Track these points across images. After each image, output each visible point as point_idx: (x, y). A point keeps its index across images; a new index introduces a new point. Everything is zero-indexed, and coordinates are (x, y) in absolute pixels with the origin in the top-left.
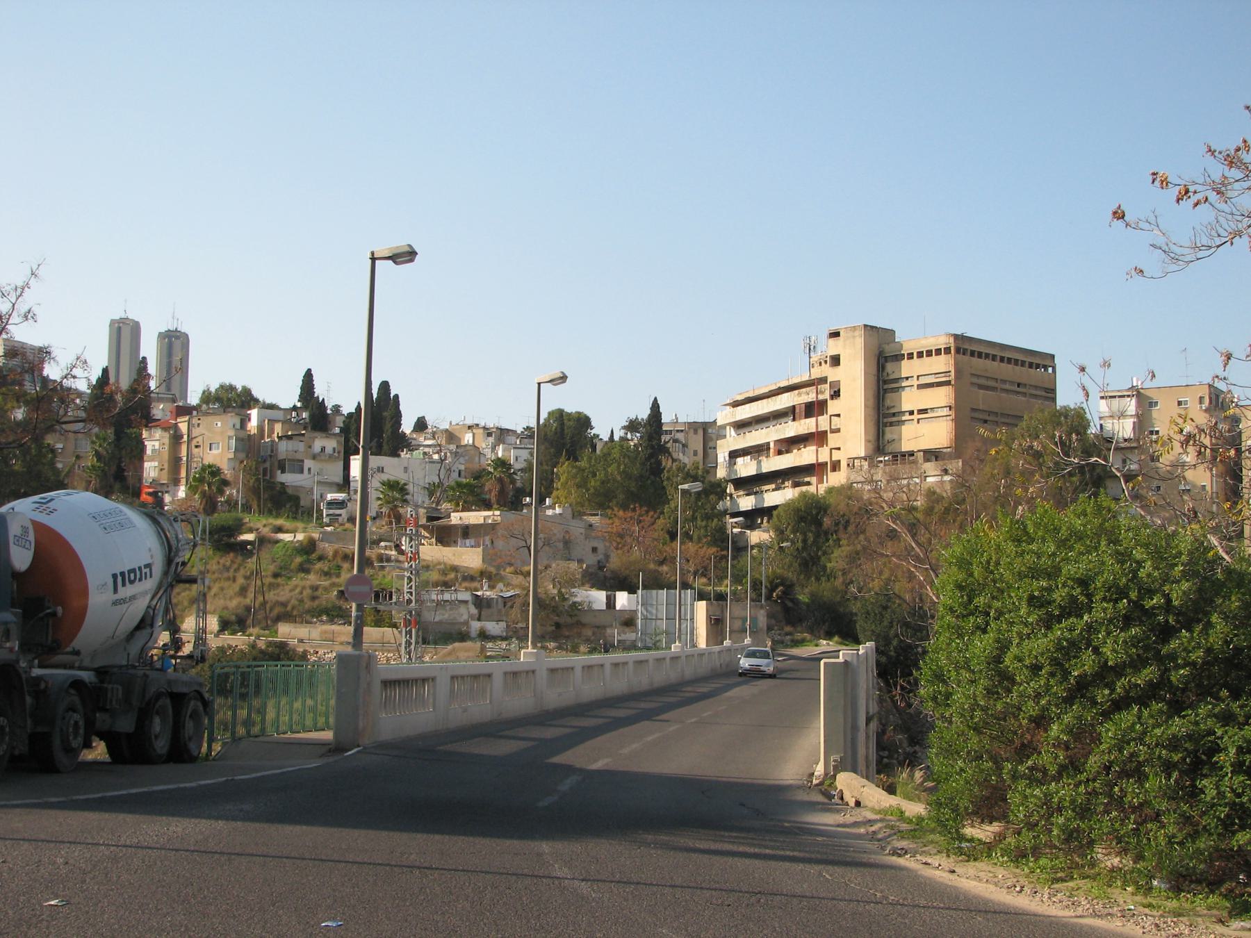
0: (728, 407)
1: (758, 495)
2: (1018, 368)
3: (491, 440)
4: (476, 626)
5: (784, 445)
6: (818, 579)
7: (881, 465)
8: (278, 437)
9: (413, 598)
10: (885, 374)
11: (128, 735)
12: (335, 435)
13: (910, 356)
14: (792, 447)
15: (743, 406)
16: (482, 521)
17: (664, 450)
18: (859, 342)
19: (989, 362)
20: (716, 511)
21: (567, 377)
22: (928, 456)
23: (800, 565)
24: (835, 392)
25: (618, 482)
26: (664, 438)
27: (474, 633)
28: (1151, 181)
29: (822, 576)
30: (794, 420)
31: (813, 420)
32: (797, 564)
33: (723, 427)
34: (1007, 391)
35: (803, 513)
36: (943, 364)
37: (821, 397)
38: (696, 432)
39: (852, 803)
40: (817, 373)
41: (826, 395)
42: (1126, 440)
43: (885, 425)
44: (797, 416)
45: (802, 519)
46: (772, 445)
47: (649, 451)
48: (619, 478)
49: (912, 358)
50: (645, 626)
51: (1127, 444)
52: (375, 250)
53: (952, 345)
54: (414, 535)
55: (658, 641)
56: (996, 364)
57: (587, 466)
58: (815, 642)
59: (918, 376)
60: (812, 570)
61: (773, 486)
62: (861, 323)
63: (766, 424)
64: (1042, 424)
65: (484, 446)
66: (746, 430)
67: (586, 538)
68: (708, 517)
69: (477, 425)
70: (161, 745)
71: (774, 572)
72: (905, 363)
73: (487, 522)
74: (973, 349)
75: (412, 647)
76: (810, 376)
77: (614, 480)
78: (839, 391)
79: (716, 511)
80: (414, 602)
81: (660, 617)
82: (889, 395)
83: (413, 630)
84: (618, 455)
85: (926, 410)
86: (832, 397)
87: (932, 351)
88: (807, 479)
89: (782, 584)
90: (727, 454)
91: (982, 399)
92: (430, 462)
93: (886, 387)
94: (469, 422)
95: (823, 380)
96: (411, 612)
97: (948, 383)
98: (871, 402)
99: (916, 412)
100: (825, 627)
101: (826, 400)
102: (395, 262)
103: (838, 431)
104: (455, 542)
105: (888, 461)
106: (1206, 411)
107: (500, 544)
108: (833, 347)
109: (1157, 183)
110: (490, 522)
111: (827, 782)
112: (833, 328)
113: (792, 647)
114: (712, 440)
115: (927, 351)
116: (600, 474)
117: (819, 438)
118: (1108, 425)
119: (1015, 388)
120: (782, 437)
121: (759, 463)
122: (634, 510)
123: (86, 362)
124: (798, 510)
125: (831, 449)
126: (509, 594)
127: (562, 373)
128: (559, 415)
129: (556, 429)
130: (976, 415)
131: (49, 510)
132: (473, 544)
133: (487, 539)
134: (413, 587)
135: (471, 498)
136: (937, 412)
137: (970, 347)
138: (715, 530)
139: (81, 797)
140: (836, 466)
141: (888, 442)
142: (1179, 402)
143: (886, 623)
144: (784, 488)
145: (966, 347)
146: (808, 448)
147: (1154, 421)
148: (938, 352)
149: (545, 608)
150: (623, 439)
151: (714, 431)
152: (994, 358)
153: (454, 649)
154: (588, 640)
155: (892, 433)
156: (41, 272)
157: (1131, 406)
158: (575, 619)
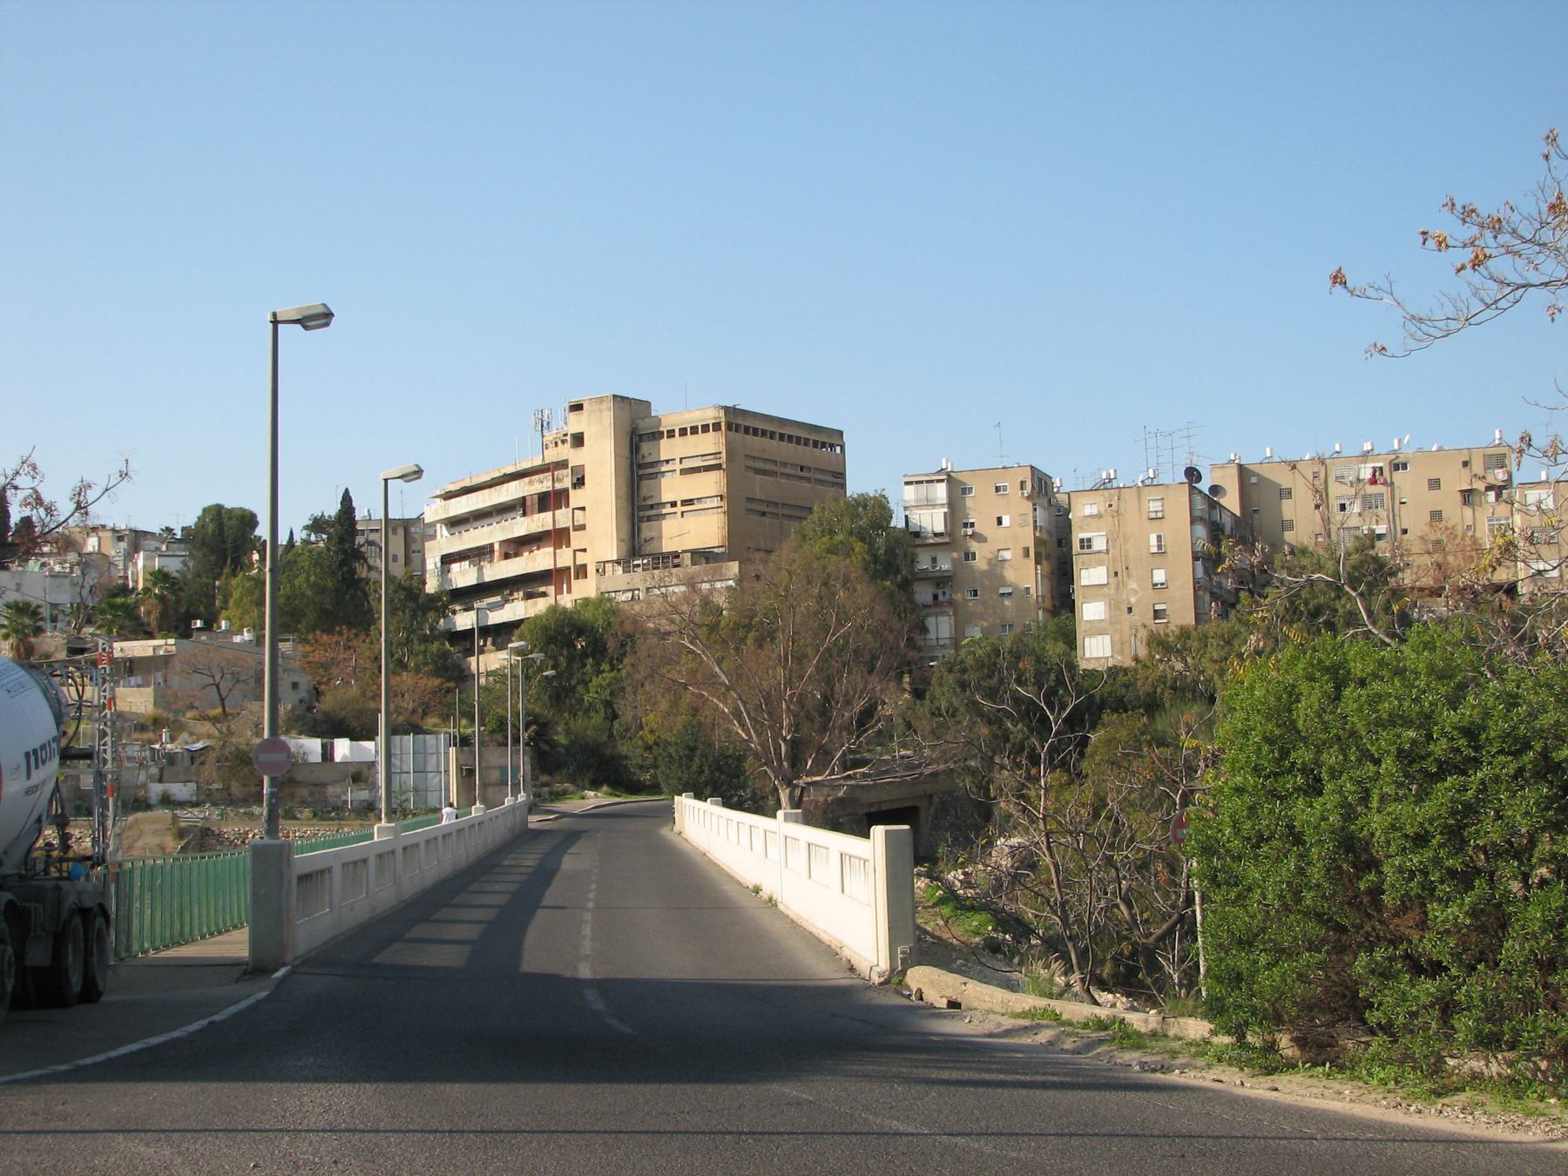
0: (438, 500)
2: (801, 448)
3: (123, 545)
4: (156, 789)
5: (512, 546)
7: (640, 569)
10: (640, 456)
13: (671, 434)
14: (523, 548)
15: (458, 499)
16: (150, 653)
17: (358, 555)
18: (608, 417)
19: (766, 441)
23: (550, 697)
24: (578, 479)
25: (308, 598)
26: (360, 540)
27: (154, 799)
28: (1421, 242)
29: (579, 710)
30: (524, 514)
31: (550, 514)
32: (546, 697)
33: (433, 524)
34: (789, 476)
36: (711, 443)
37: (558, 486)
38: (395, 531)
39: (943, 1003)
40: (552, 455)
41: (567, 483)
42: (936, 535)
43: (641, 520)
44: (528, 510)
45: (551, 640)
46: (497, 547)
47: (341, 557)
49: (674, 436)
51: (939, 540)
52: (278, 311)
53: (723, 420)
54: (108, 675)
56: (774, 443)
59: (681, 459)
62: (609, 394)
63: (489, 521)
64: (837, 516)
65: (113, 553)
69: (104, 527)
70: (76, 982)
72: (664, 443)
73: (157, 654)
76: (543, 459)
77: (303, 595)
78: (583, 477)
80: (110, 762)
82: (645, 483)
83: (111, 799)
85: (692, 500)
86: (575, 486)
87: (697, 427)
88: (542, 589)
89: (535, 722)
90: (438, 560)
91: (760, 486)
92: (51, 576)
93: (641, 472)
95: (563, 464)
97: (717, 467)
98: (624, 489)
99: (679, 503)
100: (590, 775)
101: (566, 490)
102: (306, 328)
103: (582, 527)
105: (648, 564)
106: (1028, 498)
107: (176, 681)
108: (575, 424)
109: (1431, 243)
110: (162, 653)
111: (895, 980)
112: (575, 400)
113: (552, 801)
117: (558, 537)
120: (510, 536)
121: (480, 569)
122: (340, 633)
123: (34, 468)
124: (546, 628)
125: (575, 551)
126: (199, 745)
127: (417, 466)
129: (213, 531)
132: (140, 682)
134: (109, 744)
136: (705, 502)
137: (744, 423)
139: (89, 1061)
140: (582, 571)
141: (646, 541)
142: (997, 488)
143: (694, 768)
145: (739, 422)
146: (542, 550)
147: (968, 511)
148: (705, 428)
150: (306, 542)
151: (418, 530)
153: (136, 820)
154: (304, 803)
157: (941, 491)
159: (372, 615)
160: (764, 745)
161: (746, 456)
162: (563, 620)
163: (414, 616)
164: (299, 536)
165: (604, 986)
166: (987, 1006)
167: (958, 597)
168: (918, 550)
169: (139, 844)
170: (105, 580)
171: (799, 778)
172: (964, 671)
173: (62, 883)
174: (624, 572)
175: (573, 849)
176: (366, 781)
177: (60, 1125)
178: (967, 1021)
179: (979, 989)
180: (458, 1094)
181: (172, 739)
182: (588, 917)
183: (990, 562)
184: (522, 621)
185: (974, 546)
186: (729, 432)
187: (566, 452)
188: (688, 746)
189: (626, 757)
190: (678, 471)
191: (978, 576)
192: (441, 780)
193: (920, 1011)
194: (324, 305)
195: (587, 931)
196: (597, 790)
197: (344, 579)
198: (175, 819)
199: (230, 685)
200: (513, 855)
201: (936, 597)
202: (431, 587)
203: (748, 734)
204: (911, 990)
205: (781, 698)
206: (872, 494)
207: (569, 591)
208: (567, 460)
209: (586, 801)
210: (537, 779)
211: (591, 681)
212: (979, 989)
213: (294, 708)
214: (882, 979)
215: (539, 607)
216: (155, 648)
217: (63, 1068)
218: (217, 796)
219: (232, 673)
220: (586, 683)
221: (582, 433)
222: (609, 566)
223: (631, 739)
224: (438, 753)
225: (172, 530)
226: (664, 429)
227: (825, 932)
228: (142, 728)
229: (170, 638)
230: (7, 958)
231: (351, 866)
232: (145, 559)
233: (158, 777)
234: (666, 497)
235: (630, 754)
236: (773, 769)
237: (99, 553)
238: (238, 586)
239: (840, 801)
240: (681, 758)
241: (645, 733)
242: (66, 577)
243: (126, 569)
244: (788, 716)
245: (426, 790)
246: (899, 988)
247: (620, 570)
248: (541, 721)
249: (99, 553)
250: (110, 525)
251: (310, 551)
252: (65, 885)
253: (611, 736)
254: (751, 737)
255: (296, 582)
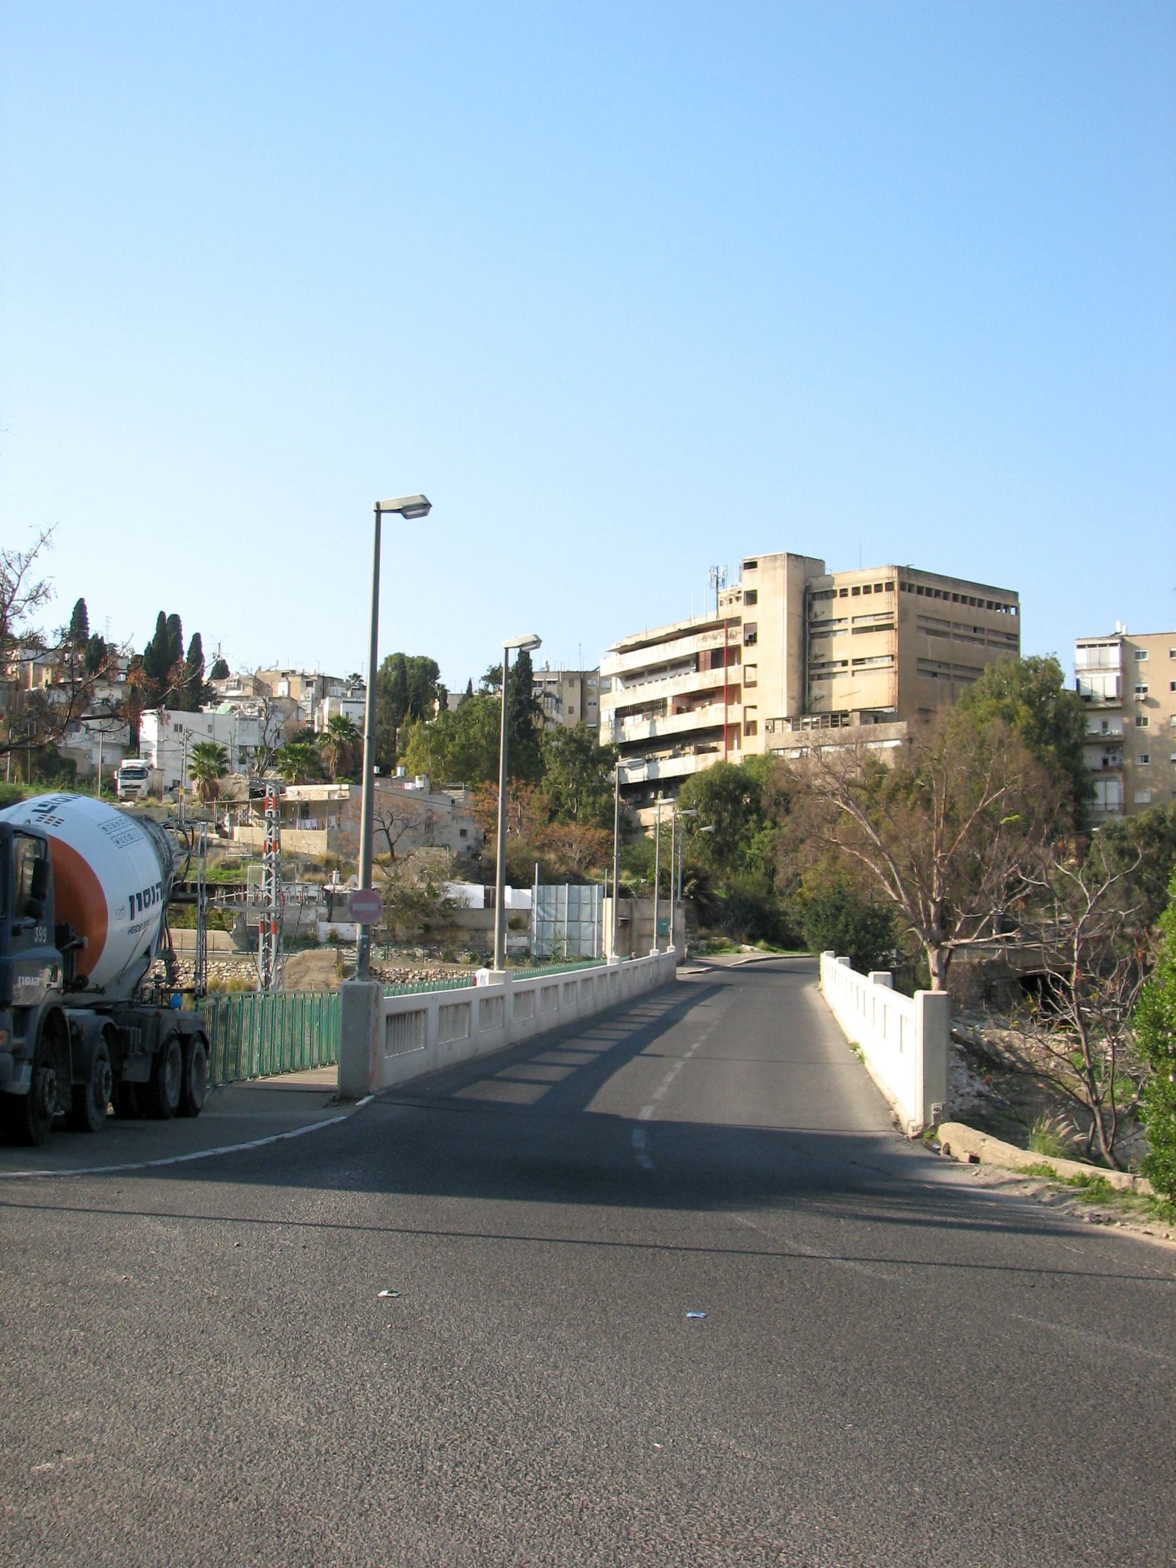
0: (614, 654)
1: (652, 764)
2: (974, 609)
3: (311, 690)
4: (325, 928)
5: (685, 701)
6: (735, 869)
7: (808, 728)
8: (47, 685)
9: (273, 897)
10: (812, 615)
11: (138, 1085)
12: (120, 683)
14: (696, 703)
16: (325, 797)
17: (535, 707)
19: (939, 602)
20: (605, 784)
21: (541, 641)
22: (865, 717)
23: (713, 852)
24: (750, 637)
25: (482, 746)
26: (536, 691)
29: (740, 865)
30: (697, 670)
33: (608, 678)
34: (961, 637)
35: (717, 788)
37: (731, 643)
38: (572, 684)
39: (965, 1158)
40: (726, 612)
41: (739, 640)
42: (1108, 699)
43: (812, 678)
44: (701, 665)
46: (669, 702)
47: (517, 708)
48: (484, 743)
50: (541, 930)
51: (1109, 704)
52: (381, 501)
54: (274, 819)
55: (559, 949)
56: (948, 603)
57: (444, 727)
58: (737, 948)
59: (853, 618)
60: (727, 858)
61: (670, 752)
62: (784, 552)
63: (663, 675)
64: (1006, 679)
65: (302, 698)
66: (636, 682)
67: (453, 818)
68: (595, 792)
69: (293, 672)
70: (172, 1097)
71: (685, 862)
72: (837, 601)
73: (332, 798)
74: (921, 584)
75: (272, 958)
77: (478, 745)
78: (755, 635)
79: (605, 784)
80: (274, 901)
81: (560, 918)
83: (273, 936)
84: (482, 713)
86: (747, 643)
89: (695, 876)
91: (932, 647)
93: (813, 631)
94: (283, 668)
95: (735, 621)
96: (269, 915)
97: (888, 627)
98: (796, 649)
99: (850, 662)
100: (748, 930)
102: (406, 517)
103: (753, 684)
104: (291, 823)
105: (817, 723)
108: (750, 581)
110: (336, 797)
111: (927, 1135)
112: (749, 558)
113: (709, 954)
114: (592, 694)
115: (865, 587)
116: (460, 738)
117: (729, 693)
118: (1086, 680)
119: (971, 634)
121: (653, 723)
124: (711, 784)
125: (745, 708)
127: (536, 636)
128: (400, 662)
130: (923, 666)
131: (55, 820)
132: (315, 825)
133: (333, 819)
134: (273, 884)
135: (306, 768)
136: (876, 662)
138: (605, 807)
139: (158, 1163)
140: (751, 727)
143: (840, 927)
144: (684, 754)
146: (715, 706)
147: (1141, 676)
148: (878, 588)
149: (412, 906)
150: (484, 693)
151: (595, 683)
152: (946, 596)
153: (304, 957)
154: (465, 946)
155: (820, 688)
156: (53, 538)
157: (1113, 656)
158: (449, 920)
159: (544, 766)
160: (913, 904)
161: (919, 616)
162: (728, 777)
163: (584, 768)
164: (478, 686)
165: (652, 1127)
166: (997, 1161)
167: (1128, 762)
168: (1088, 715)
169: (306, 979)
170: (292, 723)
171: (948, 939)
172: (1123, 838)
173: (161, 1011)
174: (793, 730)
175: (707, 1002)
176: (525, 928)
177: (107, 1207)
178: (974, 1173)
179: (994, 1146)
180: (450, 1205)
181: (342, 881)
182: (679, 1065)
183: (1161, 728)
184: (688, 776)
185: (1146, 712)
186: (902, 593)
187: (739, 609)
188: (834, 905)
189: (785, 914)
190: (850, 631)
191: (1149, 741)
192: (593, 931)
193: (935, 1164)
194: (423, 496)
195: (669, 1078)
196: (753, 944)
197: (519, 729)
198: (340, 957)
199: (399, 830)
200: (645, 1005)
201: (1105, 762)
202: (605, 738)
203: (899, 896)
204: (940, 1144)
205: (931, 863)
206: (1043, 658)
207: (739, 747)
208: (739, 618)
209: (741, 955)
210: (695, 932)
211: (753, 837)
212: (994, 1146)
213: (459, 855)
214: (916, 1133)
215: (708, 761)
216: (330, 793)
217: (135, 1166)
218: (382, 937)
219: (402, 820)
220: (748, 839)
221: (756, 591)
222: (778, 724)
223: (790, 895)
224: (592, 904)
225: (359, 676)
226: (837, 587)
227: (889, 1089)
228: (315, 869)
229: (346, 783)
230: (104, 1072)
231: (451, 1010)
232: (331, 705)
233: (327, 916)
234: (837, 656)
235: (790, 910)
236: (921, 930)
237: (289, 697)
238: (414, 735)
239: (992, 964)
240: (827, 916)
241: (804, 890)
242: (255, 720)
243: (313, 713)
244: (938, 878)
245: (580, 939)
246: (930, 1142)
247: (789, 726)
248: (702, 875)
249: (289, 697)
250: (299, 671)
251: (485, 702)
252: (165, 1013)
253: (770, 891)
254: (899, 896)
255: (471, 732)
